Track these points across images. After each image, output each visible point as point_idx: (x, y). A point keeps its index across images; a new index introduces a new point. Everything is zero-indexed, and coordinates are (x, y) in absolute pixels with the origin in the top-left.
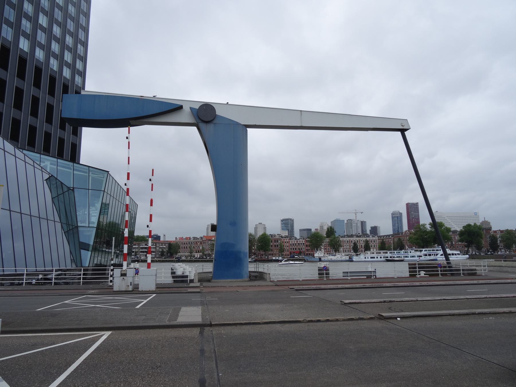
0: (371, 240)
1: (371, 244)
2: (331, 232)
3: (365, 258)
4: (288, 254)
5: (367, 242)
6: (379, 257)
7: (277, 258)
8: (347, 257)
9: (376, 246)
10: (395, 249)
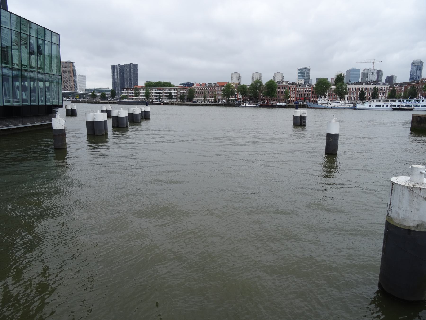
0: (381, 88)
1: (381, 92)
2: (340, 79)
3: (370, 106)
4: (294, 100)
5: (375, 90)
6: (385, 106)
7: (281, 104)
8: (351, 104)
9: (386, 94)
10: (405, 97)
